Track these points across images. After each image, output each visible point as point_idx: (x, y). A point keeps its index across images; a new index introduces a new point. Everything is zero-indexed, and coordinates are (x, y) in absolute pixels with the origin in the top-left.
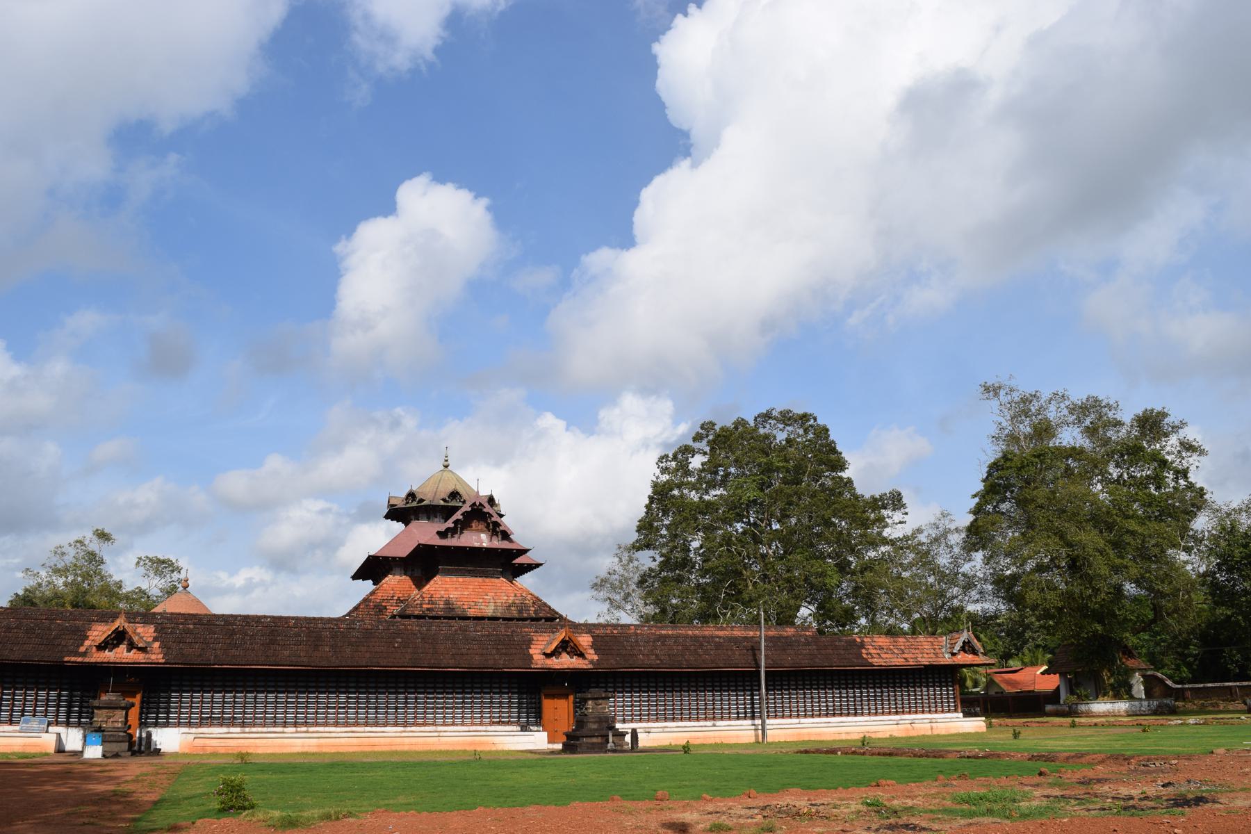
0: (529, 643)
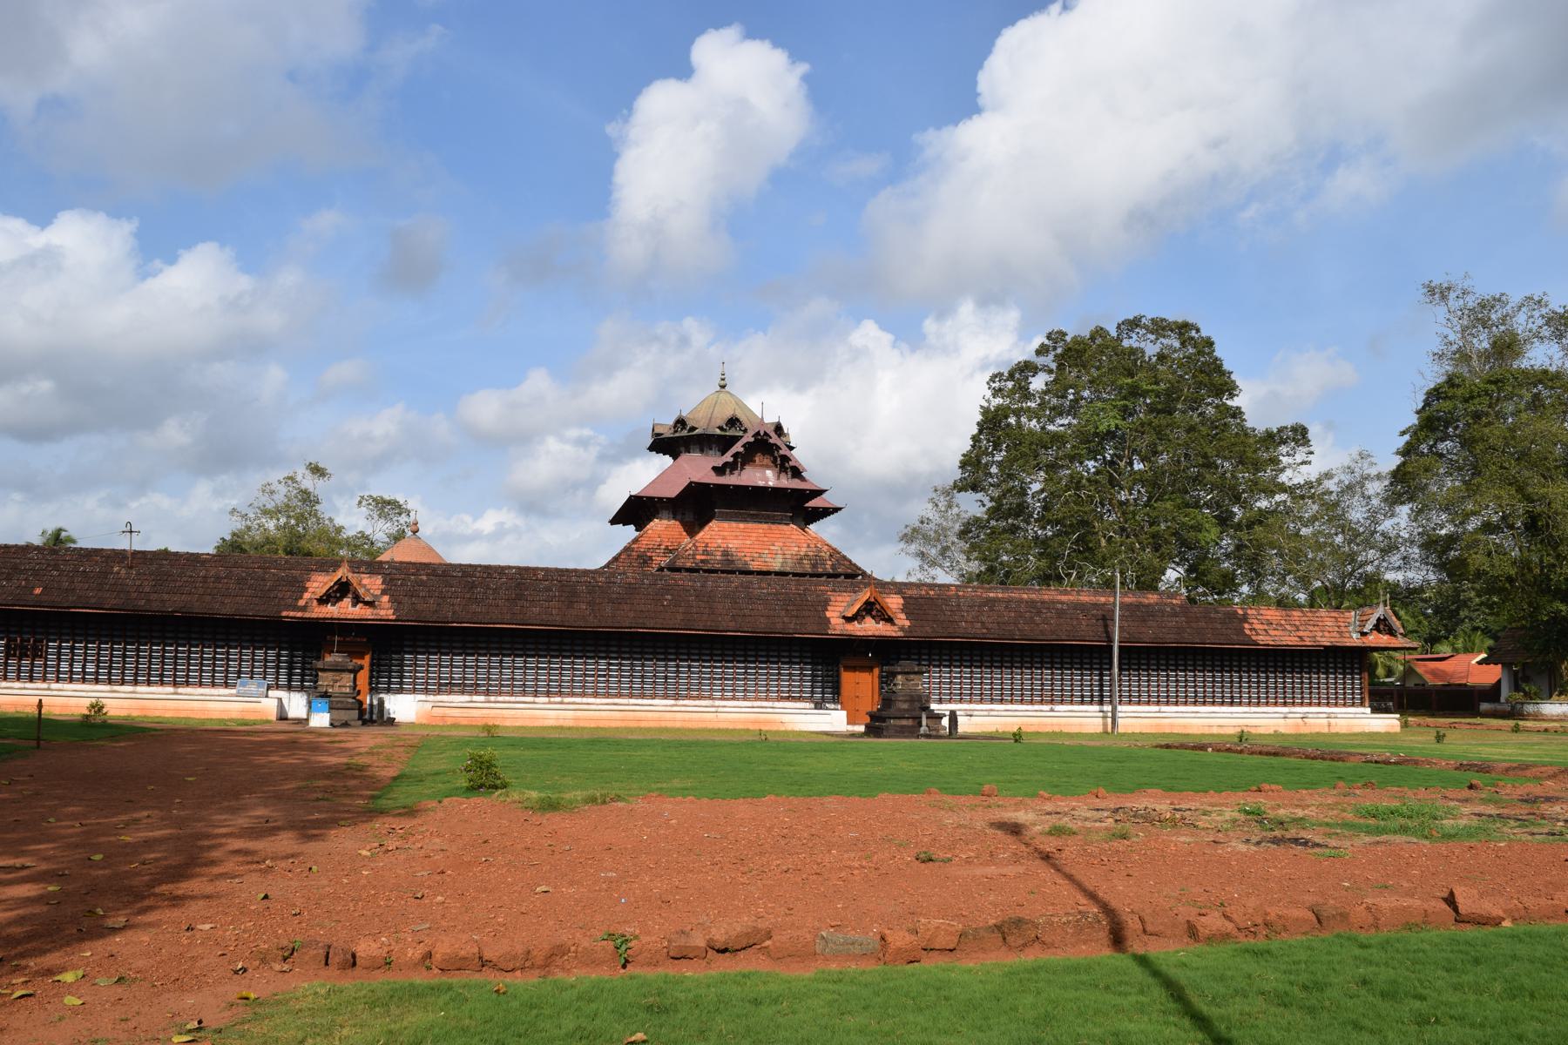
0: (826, 603)
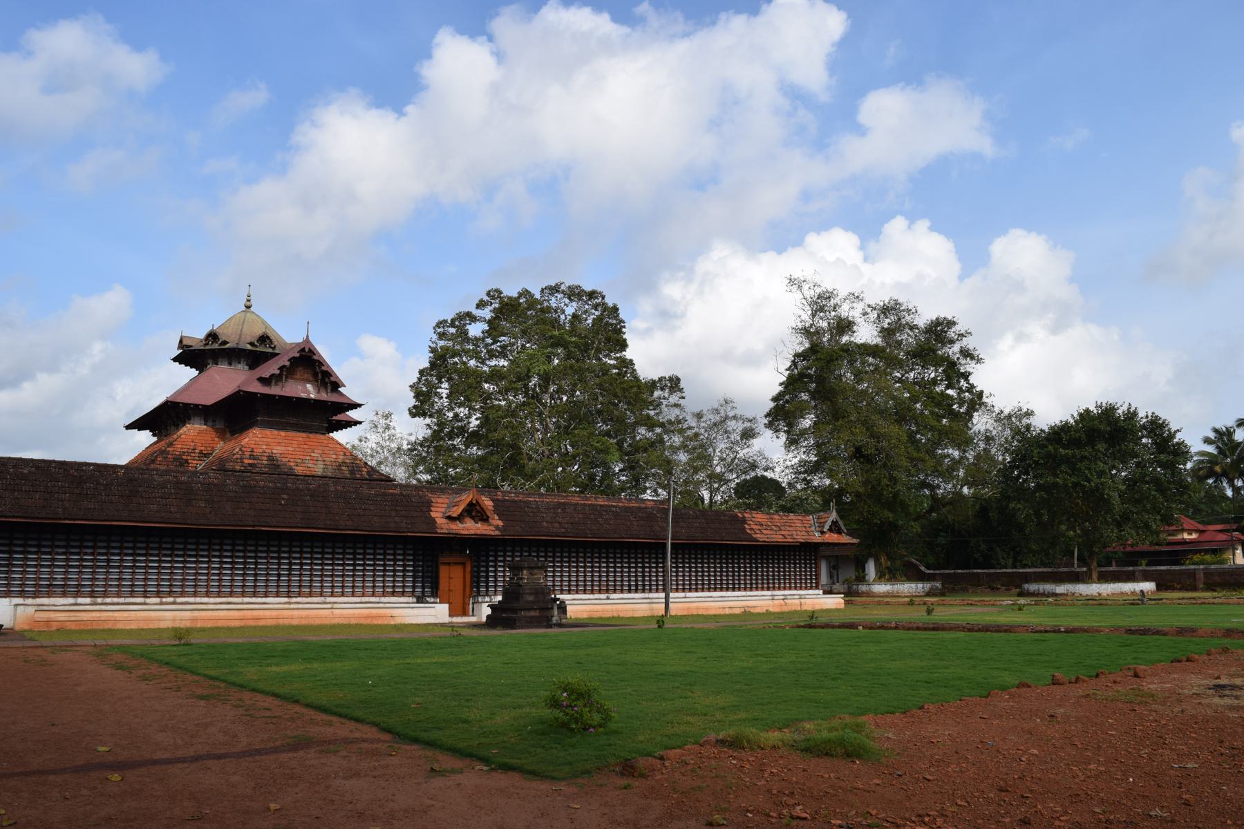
0: (429, 505)
